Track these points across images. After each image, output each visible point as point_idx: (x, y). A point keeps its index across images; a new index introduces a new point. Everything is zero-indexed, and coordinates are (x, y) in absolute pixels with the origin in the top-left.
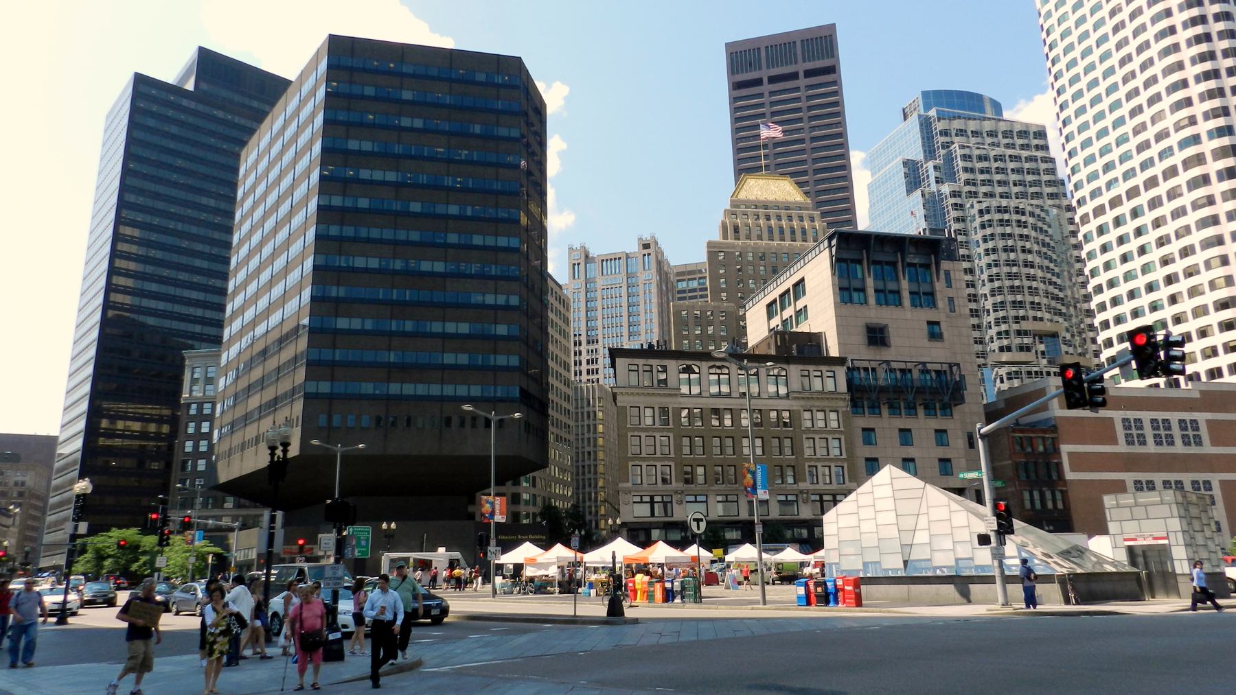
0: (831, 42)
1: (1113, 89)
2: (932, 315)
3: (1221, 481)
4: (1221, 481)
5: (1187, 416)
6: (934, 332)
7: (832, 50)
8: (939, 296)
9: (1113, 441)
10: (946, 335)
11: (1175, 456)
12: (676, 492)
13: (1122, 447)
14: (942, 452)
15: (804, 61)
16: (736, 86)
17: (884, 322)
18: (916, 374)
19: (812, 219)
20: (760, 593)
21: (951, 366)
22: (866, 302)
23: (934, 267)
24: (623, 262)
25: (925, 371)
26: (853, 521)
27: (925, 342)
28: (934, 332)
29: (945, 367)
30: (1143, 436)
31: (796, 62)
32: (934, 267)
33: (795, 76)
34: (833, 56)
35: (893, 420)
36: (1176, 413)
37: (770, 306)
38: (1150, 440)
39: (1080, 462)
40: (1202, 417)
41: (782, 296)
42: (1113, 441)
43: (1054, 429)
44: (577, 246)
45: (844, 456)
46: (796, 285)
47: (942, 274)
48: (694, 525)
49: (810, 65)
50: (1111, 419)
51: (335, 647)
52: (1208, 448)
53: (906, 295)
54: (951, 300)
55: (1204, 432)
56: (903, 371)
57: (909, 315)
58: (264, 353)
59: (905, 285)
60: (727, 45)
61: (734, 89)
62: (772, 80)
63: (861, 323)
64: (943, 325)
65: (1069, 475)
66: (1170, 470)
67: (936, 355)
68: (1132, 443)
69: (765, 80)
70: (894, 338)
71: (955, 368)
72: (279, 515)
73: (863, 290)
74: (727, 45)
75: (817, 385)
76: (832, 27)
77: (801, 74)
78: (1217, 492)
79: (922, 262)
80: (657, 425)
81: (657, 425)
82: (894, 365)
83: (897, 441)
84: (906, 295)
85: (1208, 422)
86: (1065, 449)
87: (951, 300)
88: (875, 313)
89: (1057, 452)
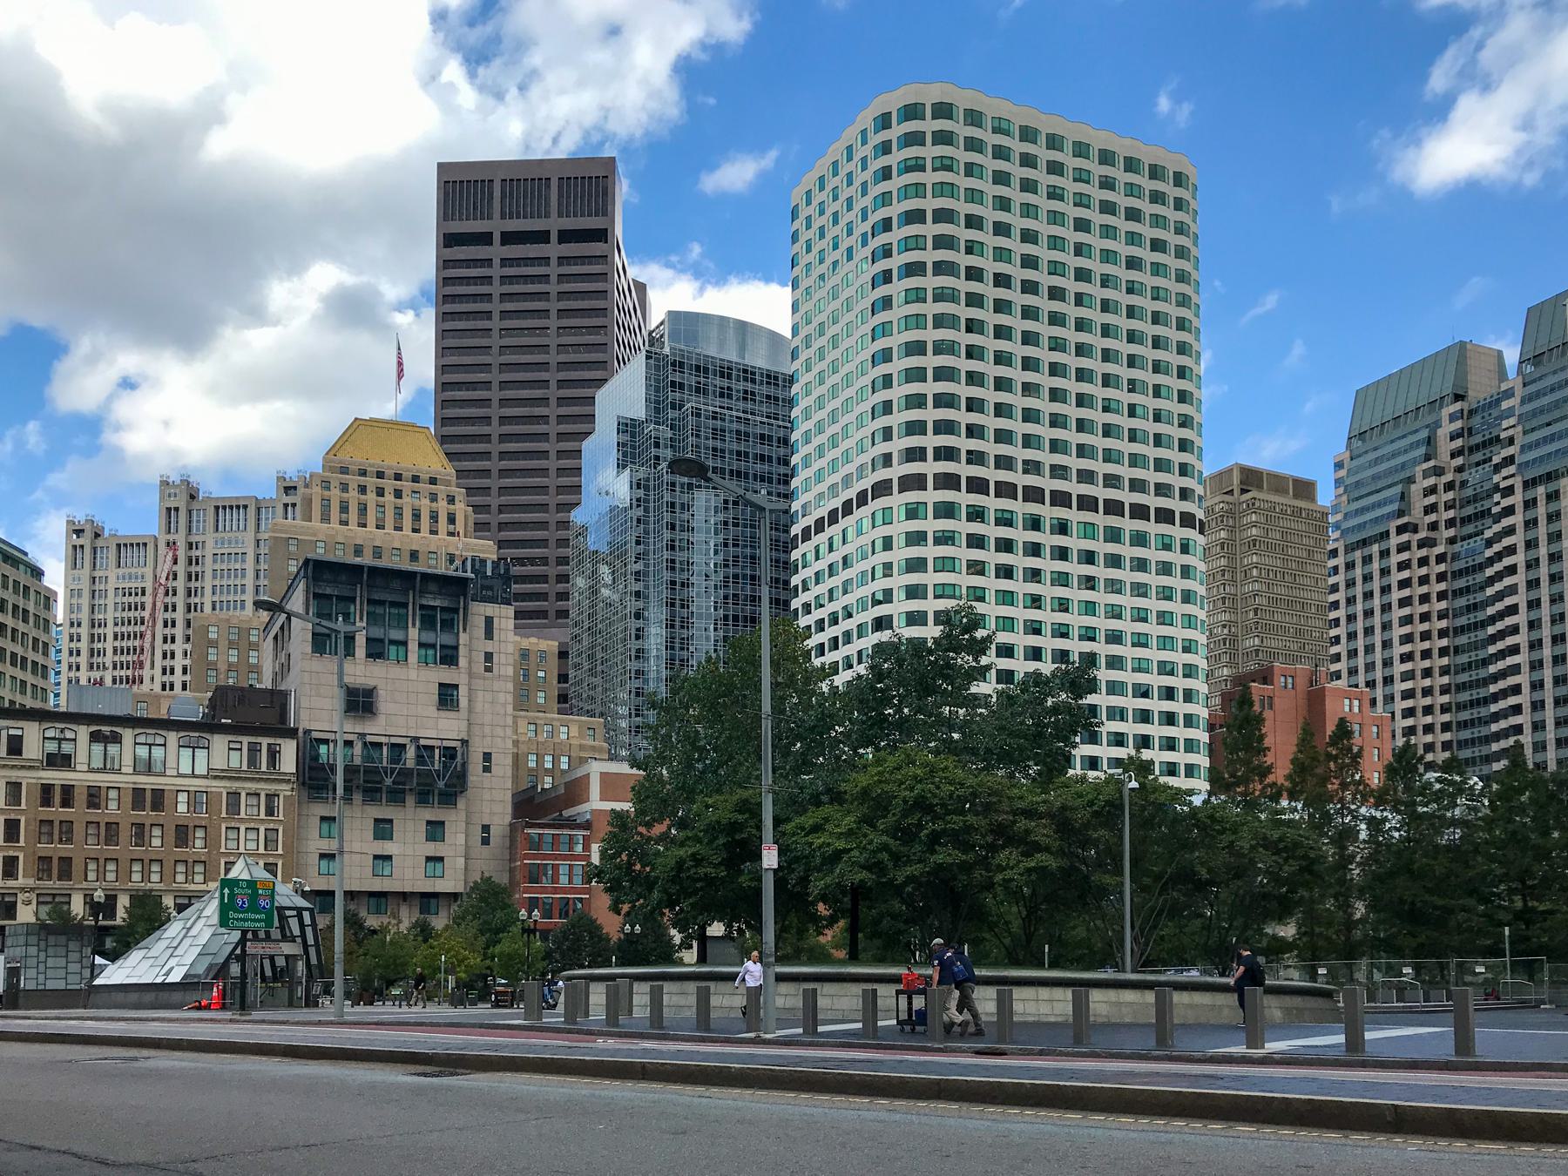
0: (605, 193)
6: (447, 697)
12: (22, 889)
14: (432, 849)
16: (448, 240)
17: (371, 683)
19: (451, 500)
24: (252, 511)
27: (432, 711)
31: (547, 216)
33: (542, 237)
34: (605, 214)
44: (174, 478)
45: (280, 851)
54: (489, 657)
57: (413, 674)
59: (414, 634)
60: (440, 165)
61: (446, 246)
62: (509, 238)
67: (444, 728)
69: (497, 238)
70: (384, 704)
72: (860, 1025)
74: (440, 165)
79: (446, 604)
87: (489, 657)
88: (361, 671)
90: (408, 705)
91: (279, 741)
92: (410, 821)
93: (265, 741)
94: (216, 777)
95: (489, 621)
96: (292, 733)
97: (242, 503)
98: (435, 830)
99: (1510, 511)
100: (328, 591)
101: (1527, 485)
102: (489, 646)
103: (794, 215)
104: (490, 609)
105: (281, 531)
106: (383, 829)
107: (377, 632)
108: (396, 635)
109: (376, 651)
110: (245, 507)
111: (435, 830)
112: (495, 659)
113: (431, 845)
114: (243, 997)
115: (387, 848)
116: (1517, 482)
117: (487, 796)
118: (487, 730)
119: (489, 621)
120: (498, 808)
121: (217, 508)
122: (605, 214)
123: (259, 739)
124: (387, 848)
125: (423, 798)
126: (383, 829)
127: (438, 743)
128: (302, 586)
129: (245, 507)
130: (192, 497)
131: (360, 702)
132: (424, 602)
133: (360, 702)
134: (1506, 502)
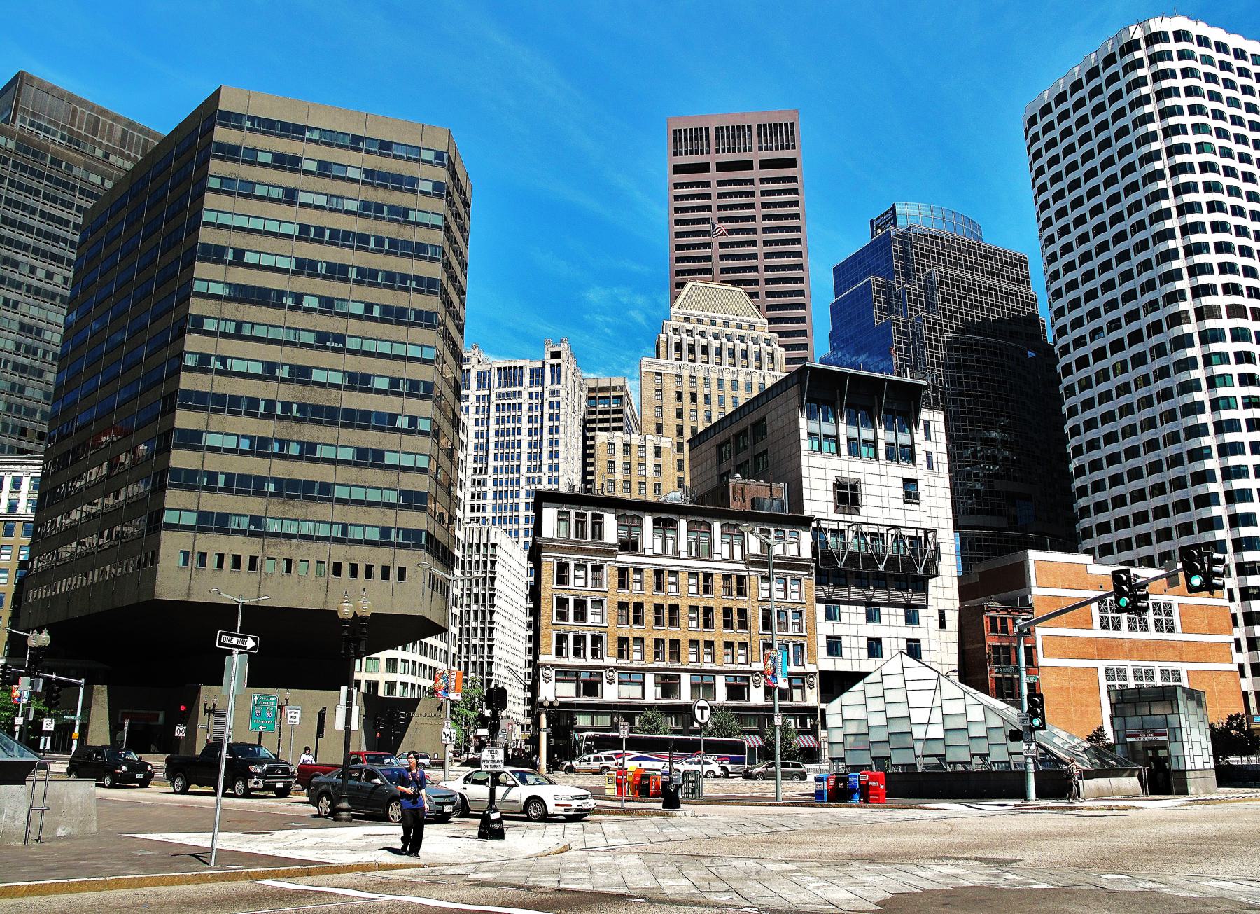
1: (1083, 121)
2: (910, 473)
6: (911, 492)
8: (918, 449)
10: (922, 496)
11: (1147, 643)
15: (760, 149)
18: (850, 536)
20: (780, 791)
21: (926, 531)
25: (899, 538)
26: (859, 713)
28: (911, 492)
37: (719, 447)
41: (737, 436)
46: (754, 425)
47: (921, 426)
48: (698, 713)
51: (497, 826)
56: (874, 536)
58: (21, 451)
63: (832, 476)
64: (921, 485)
71: (930, 535)
75: (778, 550)
77: (756, 165)
80: (589, 587)
81: (589, 587)
82: (865, 528)
83: (924, 645)
131: (847, 495)
133: (847, 495)
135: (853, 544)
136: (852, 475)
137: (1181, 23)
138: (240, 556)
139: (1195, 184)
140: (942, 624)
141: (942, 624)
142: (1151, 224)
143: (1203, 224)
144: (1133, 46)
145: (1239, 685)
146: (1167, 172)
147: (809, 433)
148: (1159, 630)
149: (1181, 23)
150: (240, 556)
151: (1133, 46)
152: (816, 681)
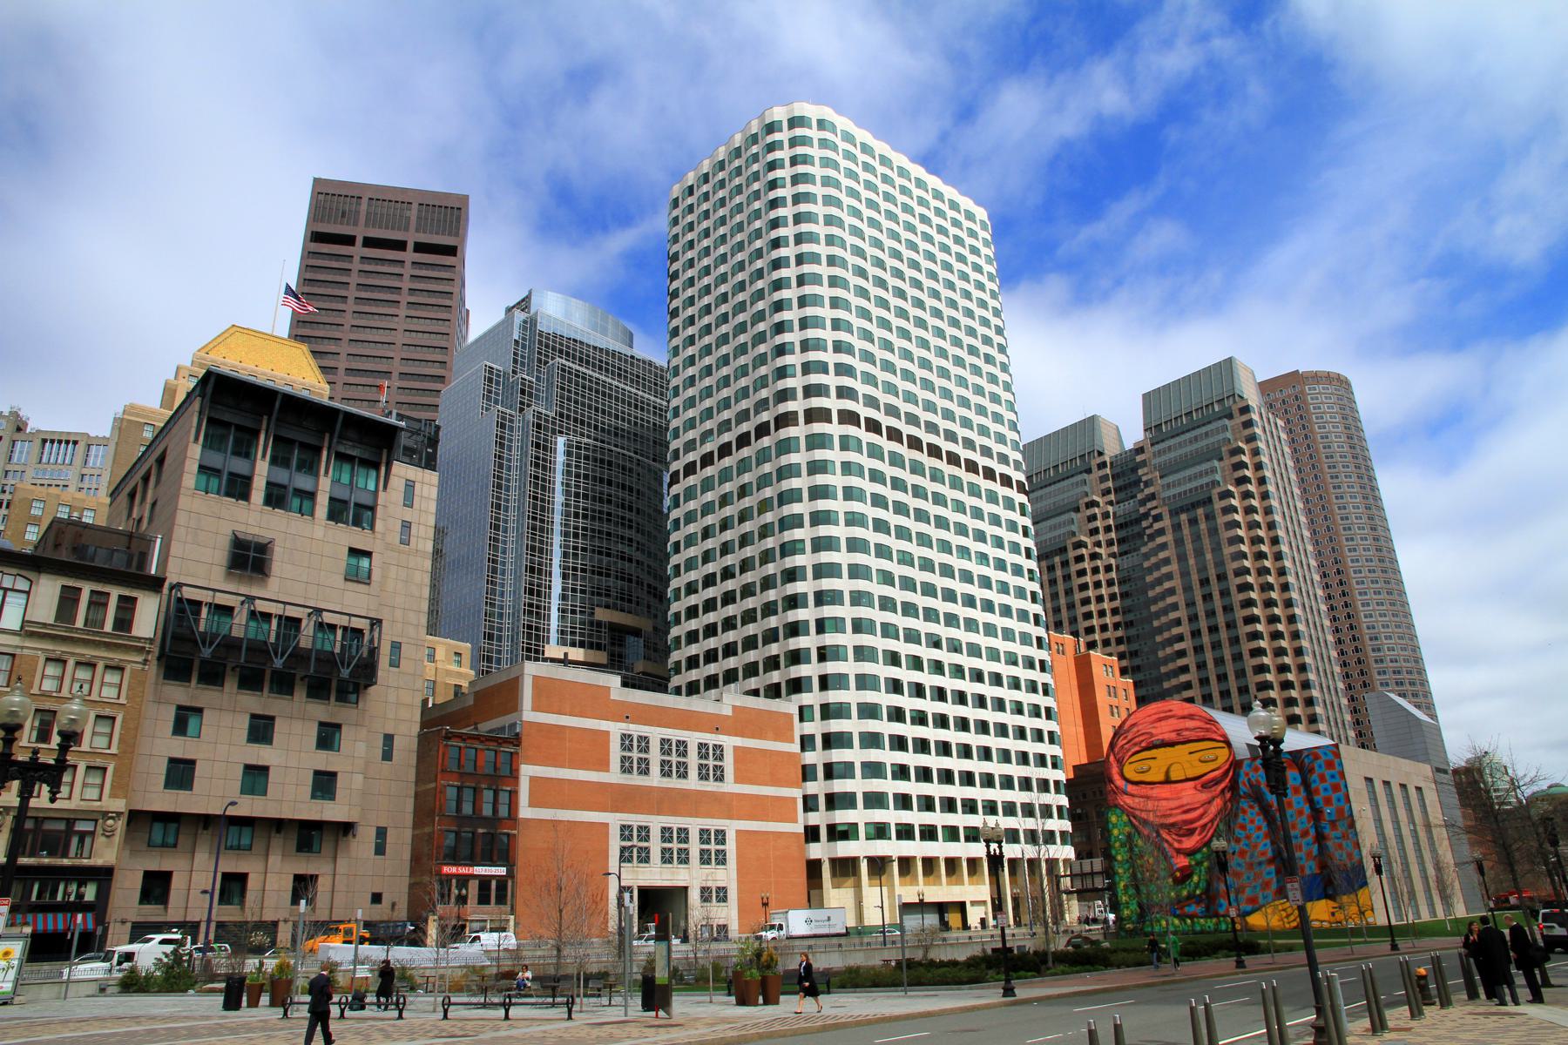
0: (458, 219)
3: (738, 832)
4: (738, 832)
5: (711, 739)
7: (458, 228)
9: (603, 765)
11: (685, 794)
13: (614, 776)
14: (324, 760)
15: (417, 231)
16: (316, 237)
18: (241, 617)
22: (312, 514)
23: (383, 469)
27: (339, 581)
29: (362, 624)
30: (685, 765)
32: (383, 469)
34: (457, 235)
35: (240, 697)
36: (659, 729)
38: (655, 768)
39: (545, 792)
40: (729, 742)
42: (603, 765)
43: (516, 740)
45: (114, 750)
49: (424, 238)
50: (607, 733)
52: (730, 786)
53: (323, 501)
54: (407, 526)
55: (728, 763)
65: (525, 812)
66: (674, 812)
68: (630, 771)
70: (279, 564)
73: (311, 496)
76: (466, 197)
77: (410, 246)
78: (731, 847)
79: (366, 456)
82: (328, 618)
84: (323, 501)
85: (736, 748)
86: (527, 771)
87: (407, 526)
88: (254, 518)
89: (514, 776)
90: (310, 567)
91: (134, 594)
92: (296, 721)
93: (115, 592)
94: (32, 635)
95: (410, 485)
96: (155, 584)
97: (72, 438)
98: (328, 736)
99: (1161, 532)
100: (226, 417)
101: (1174, 513)
102: (408, 515)
103: (675, 203)
104: (413, 472)
105: (138, 415)
106: (261, 730)
107: (282, 476)
108: (303, 481)
109: (276, 497)
110: (75, 443)
111: (328, 736)
112: (414, 531)
113: (323, 754)
114: (506, 741)
115: (260, 754)
116: (1165, 511)
117: (392, 698)
118: (398, 614)
119: (410, 485)
120: (404, 714)
121: (44, 441)
122: (457, 235)
123: (106, 589)
124: (260, 754)
125: (318, 690)
126: (261, 730)
127: (344, 621)
128: (196, 405)
129: (75, 443)
130: (19, 429)
131: (249, 558)
132: (342, 449)
133: (249, 558)
134: (1157, 526)
135: (239, 626)
136: (262, 533)
137: (828, 113)
138: (480, 902)
139: (828, 411)
140: (387, 756)
141: (387, 756)
142: (777, 429)
143: (827, 387)
144: (771, 128)
145: (803, 851)
146: (807, 519)
147: (201, 467)
148: (682, 744)
149: (828, 113)
150: (480, 902)
151: (771, 128)
152: (121, 825)
